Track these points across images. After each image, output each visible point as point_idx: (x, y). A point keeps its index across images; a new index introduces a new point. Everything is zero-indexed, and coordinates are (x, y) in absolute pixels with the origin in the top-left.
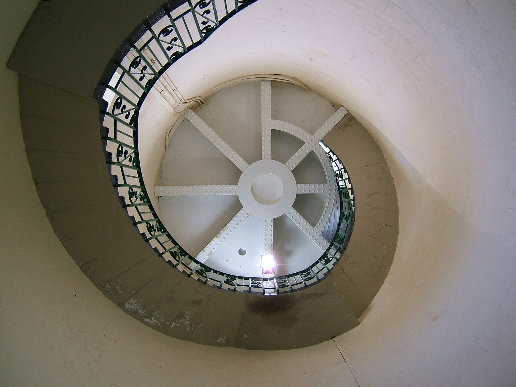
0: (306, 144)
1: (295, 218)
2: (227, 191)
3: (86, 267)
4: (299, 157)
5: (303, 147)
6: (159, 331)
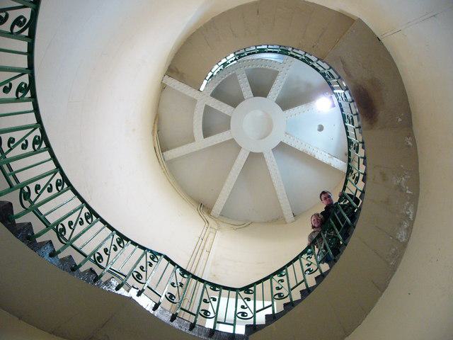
1: (275, 92)
2: (271, 159)
3: (381, 287)
5: (210, 105)
6: (417, 203)
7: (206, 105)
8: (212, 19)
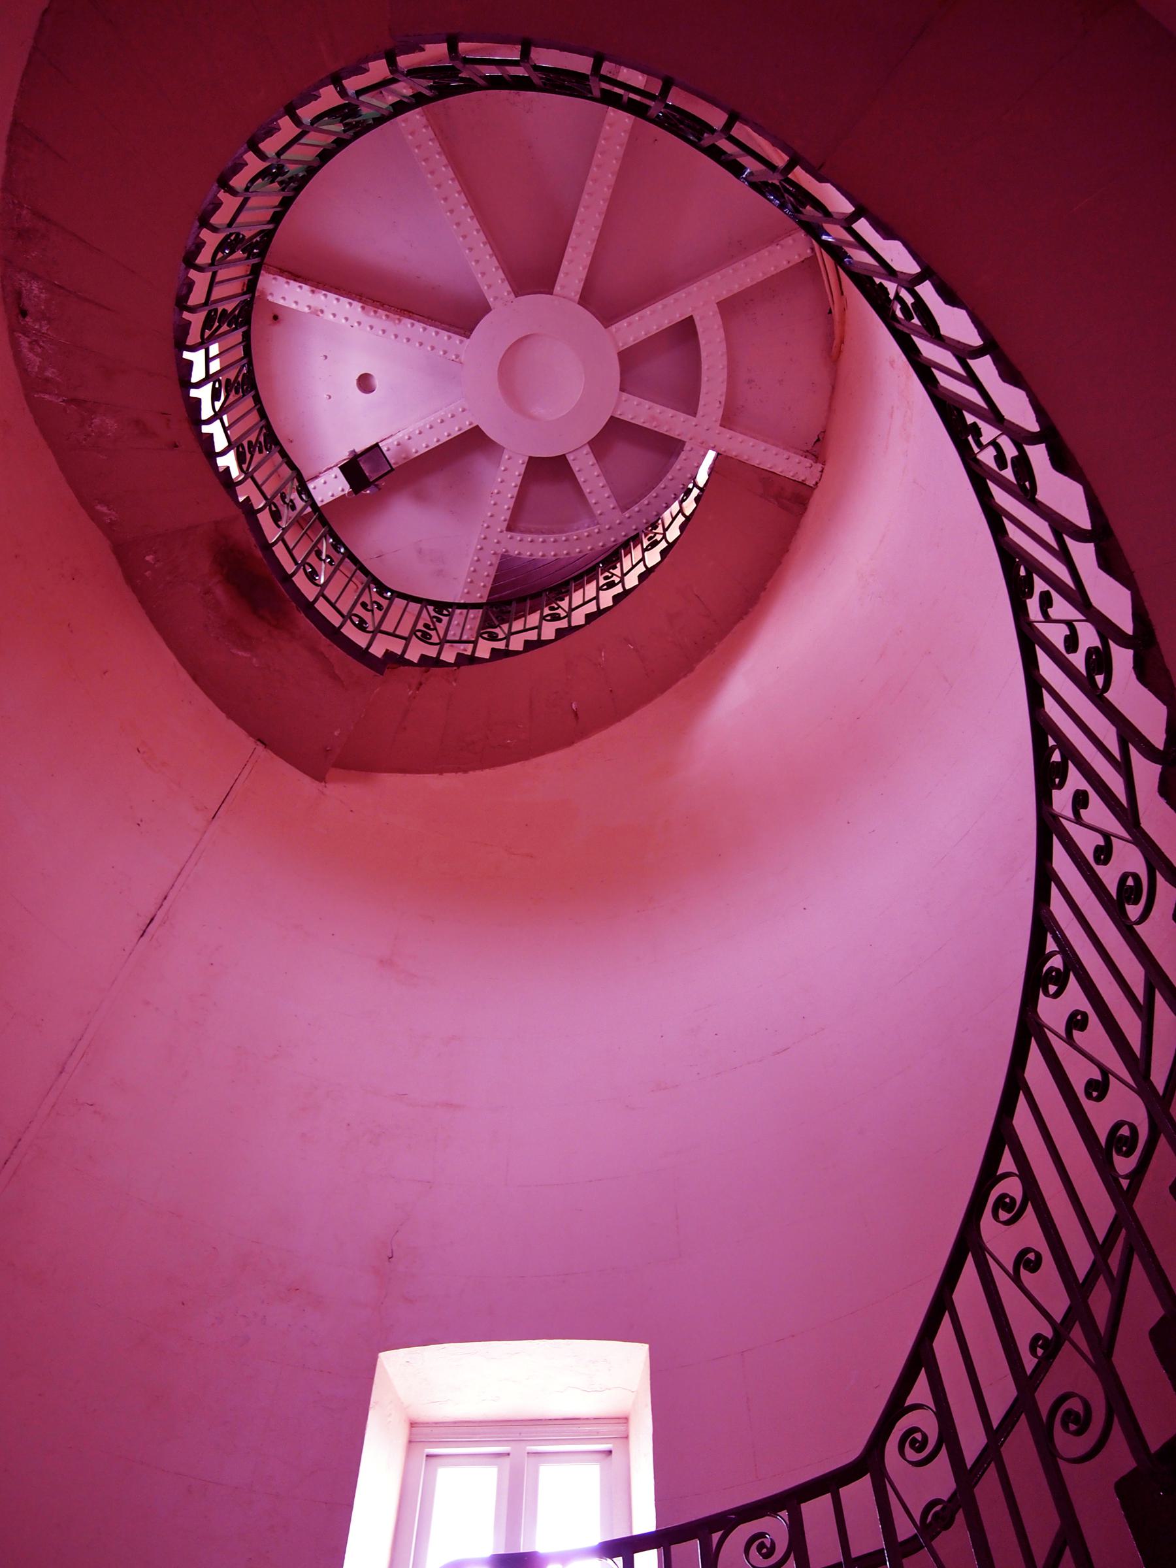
0: (693, 421)
2: (491, 280)
4: (653, 418)
5: (682, 416)
7: (694, 414)
8: (691, 670)
